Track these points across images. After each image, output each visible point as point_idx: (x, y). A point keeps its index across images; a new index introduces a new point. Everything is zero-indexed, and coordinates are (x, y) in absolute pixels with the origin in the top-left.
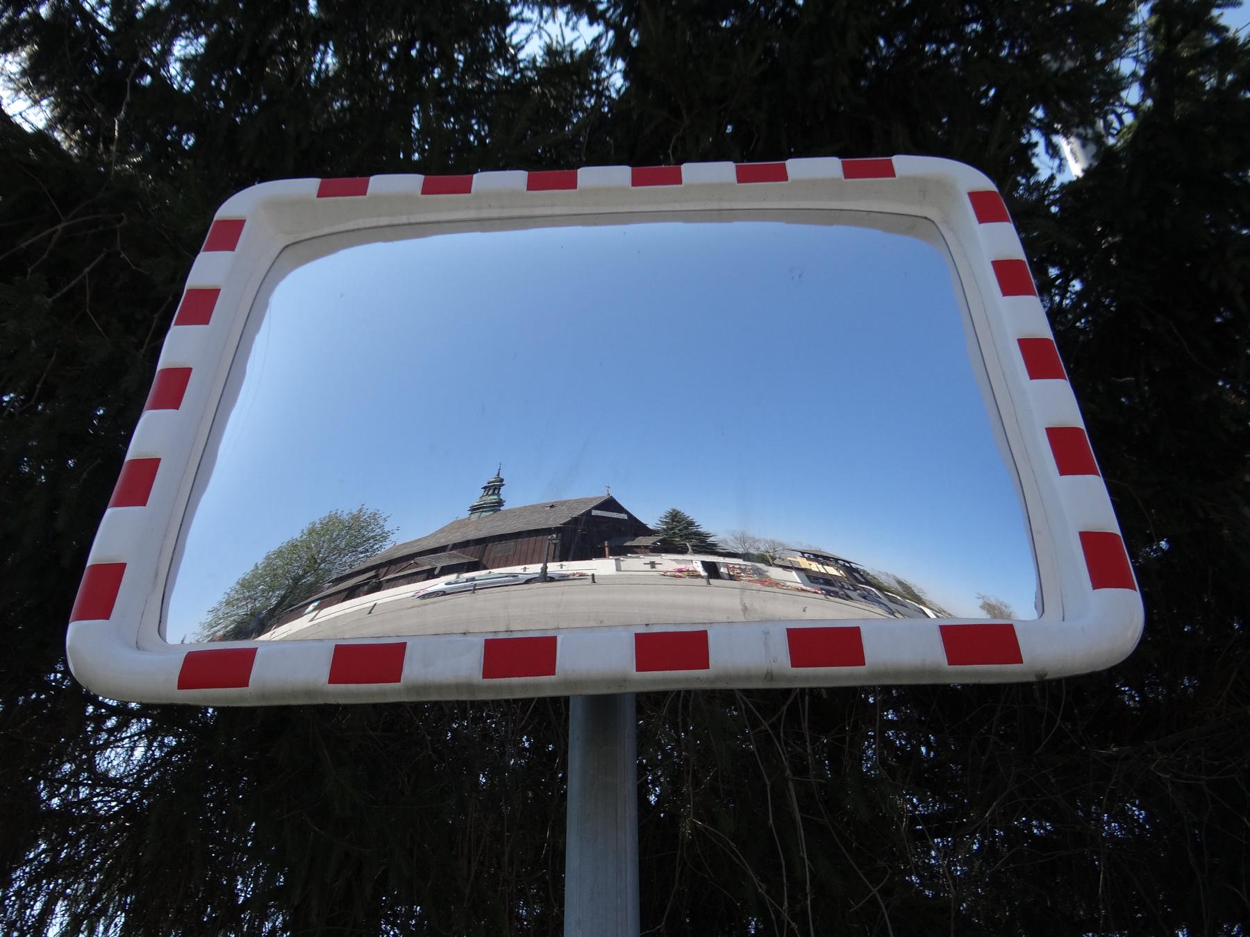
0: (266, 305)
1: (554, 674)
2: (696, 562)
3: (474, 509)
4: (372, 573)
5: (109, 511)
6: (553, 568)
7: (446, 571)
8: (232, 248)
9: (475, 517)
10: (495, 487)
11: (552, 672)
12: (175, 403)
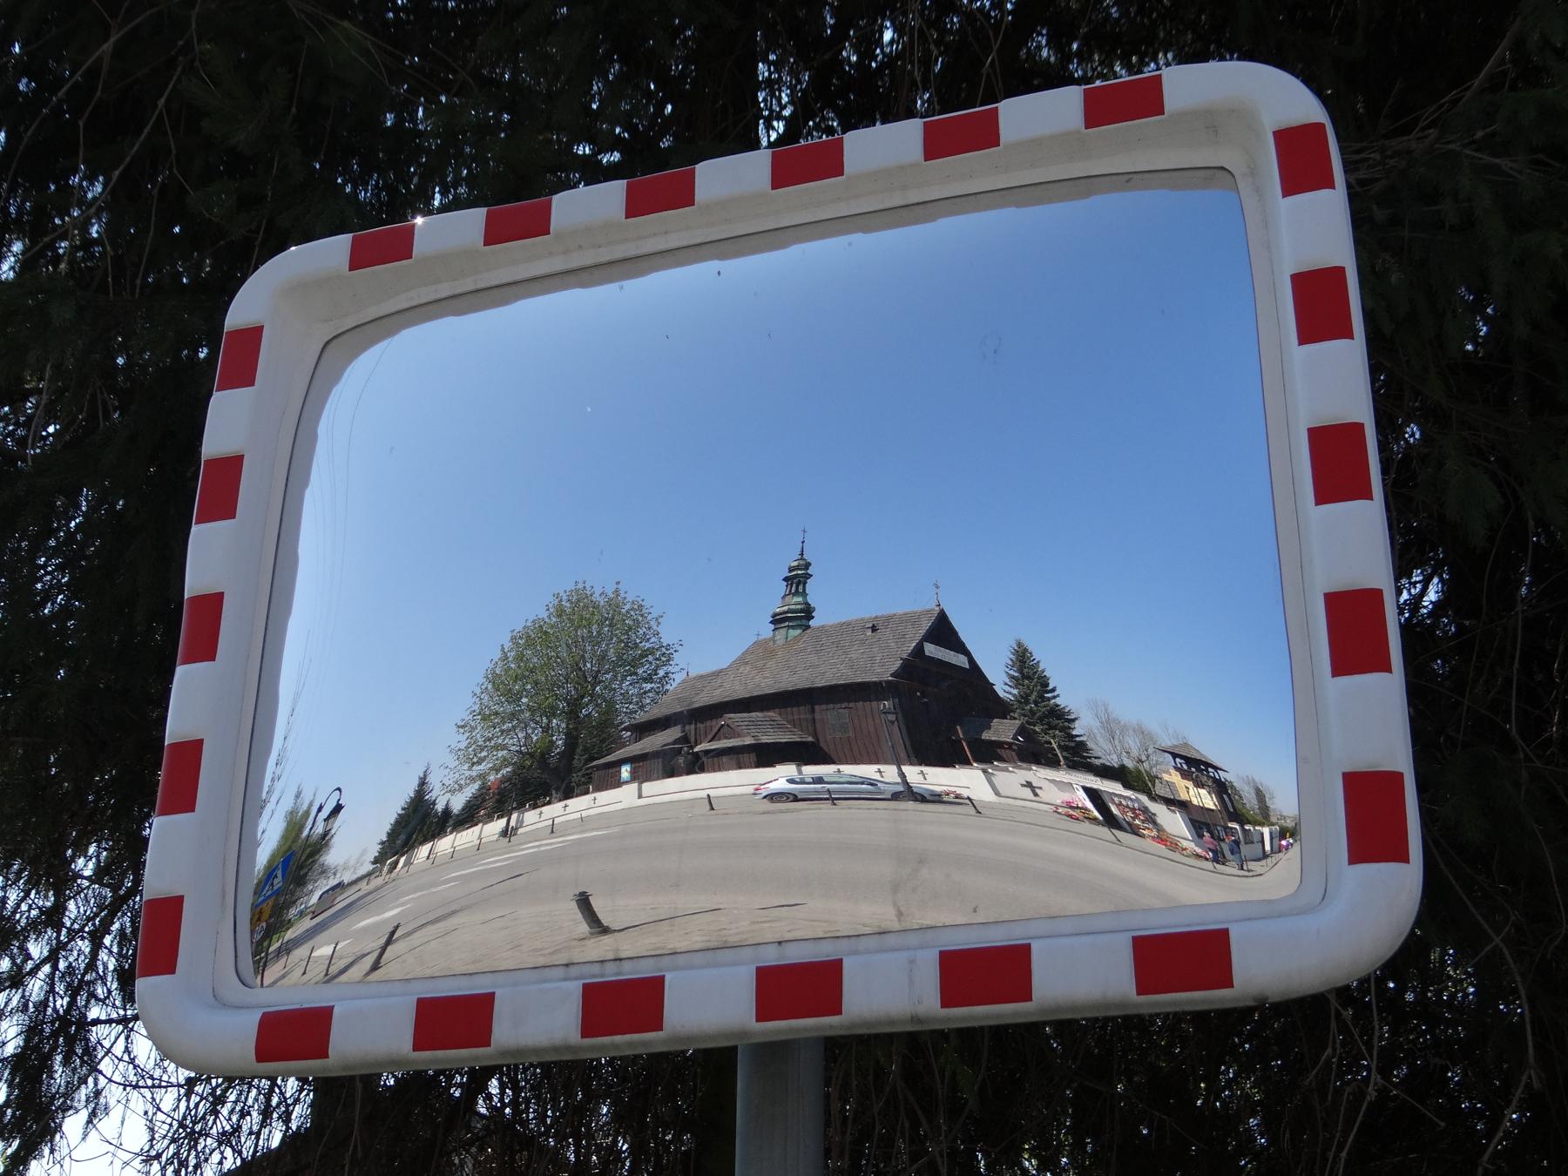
0: (314, 438)
1: (840, 1012)
2: (1063, 787)
3: (778, 620)
4: (673, 734)
5: (180, 670)
6: (913, 773)
7: (766, 756)
8: (252, 383)
9: (781, 634)
10: (797, 580)
11: (659, 1027)
12: (228, 512)
